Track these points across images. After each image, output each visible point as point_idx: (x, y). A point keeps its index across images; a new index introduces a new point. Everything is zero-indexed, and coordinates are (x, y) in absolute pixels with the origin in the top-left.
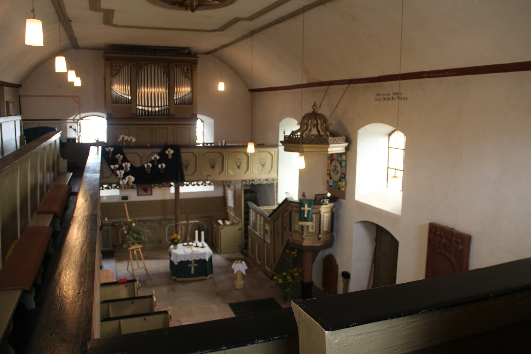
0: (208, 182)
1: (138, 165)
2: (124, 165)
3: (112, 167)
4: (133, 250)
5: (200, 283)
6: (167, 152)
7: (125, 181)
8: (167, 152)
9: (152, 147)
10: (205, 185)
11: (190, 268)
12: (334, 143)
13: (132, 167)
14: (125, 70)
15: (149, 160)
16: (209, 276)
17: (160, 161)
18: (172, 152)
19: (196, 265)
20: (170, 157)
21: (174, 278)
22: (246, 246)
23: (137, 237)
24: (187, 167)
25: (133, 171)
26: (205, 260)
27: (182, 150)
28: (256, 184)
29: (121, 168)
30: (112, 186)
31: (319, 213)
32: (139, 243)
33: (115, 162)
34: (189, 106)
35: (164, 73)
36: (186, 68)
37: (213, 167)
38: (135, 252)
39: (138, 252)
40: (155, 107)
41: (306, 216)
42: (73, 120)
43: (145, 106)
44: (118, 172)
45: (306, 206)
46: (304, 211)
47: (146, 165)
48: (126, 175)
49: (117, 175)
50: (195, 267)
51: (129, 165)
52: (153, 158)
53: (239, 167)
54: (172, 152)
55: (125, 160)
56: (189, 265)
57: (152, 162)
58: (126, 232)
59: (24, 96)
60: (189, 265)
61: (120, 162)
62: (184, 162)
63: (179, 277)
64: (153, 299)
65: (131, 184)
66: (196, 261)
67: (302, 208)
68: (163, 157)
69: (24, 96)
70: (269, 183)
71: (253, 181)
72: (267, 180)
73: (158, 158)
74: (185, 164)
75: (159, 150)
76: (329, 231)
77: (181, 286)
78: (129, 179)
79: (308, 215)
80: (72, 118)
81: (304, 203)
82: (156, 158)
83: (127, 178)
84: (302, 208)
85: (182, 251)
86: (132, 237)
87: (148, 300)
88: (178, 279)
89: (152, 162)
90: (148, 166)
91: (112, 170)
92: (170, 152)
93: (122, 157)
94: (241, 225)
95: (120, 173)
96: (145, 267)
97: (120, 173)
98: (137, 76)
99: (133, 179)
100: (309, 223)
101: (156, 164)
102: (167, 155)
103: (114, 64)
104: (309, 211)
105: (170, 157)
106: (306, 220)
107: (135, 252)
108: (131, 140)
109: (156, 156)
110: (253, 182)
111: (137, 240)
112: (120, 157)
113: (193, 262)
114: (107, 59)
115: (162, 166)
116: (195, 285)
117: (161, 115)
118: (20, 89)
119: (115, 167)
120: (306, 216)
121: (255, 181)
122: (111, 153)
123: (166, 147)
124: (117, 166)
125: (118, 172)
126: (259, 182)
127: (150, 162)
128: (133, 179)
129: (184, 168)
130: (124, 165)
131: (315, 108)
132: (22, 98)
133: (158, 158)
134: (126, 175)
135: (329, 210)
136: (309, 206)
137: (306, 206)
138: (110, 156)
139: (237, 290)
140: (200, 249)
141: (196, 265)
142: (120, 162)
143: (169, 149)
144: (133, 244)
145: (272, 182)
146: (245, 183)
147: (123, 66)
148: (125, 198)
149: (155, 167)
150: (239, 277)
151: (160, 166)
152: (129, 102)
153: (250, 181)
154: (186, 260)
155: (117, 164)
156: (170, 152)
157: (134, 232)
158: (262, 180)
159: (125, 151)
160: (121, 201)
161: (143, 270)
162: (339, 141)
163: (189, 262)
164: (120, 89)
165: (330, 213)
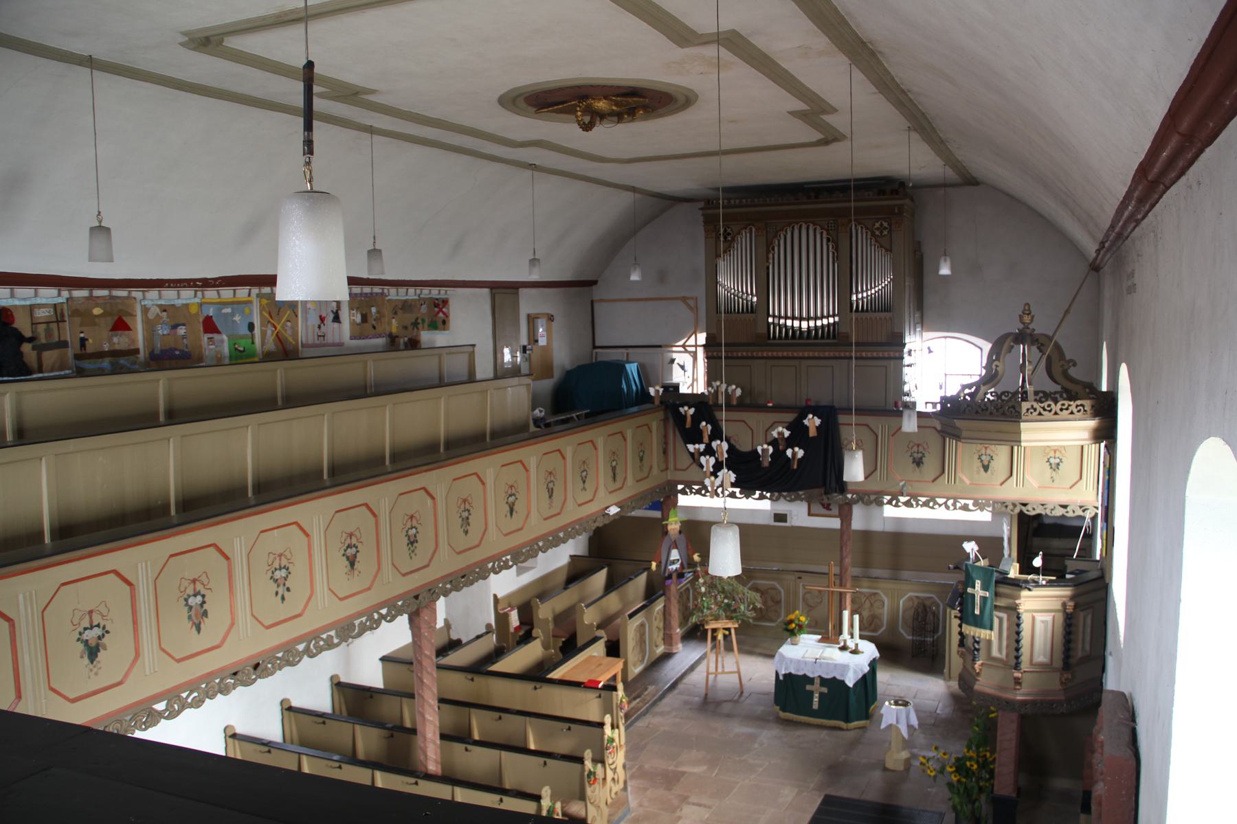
0: (903, 499)
1: (745, 447)
2: (714, 444)
3: (691, 447)
4: (714, 630)
5: (824, 734)
6: (806, 422)
8: (806, 422)
9: (778, 408)
10: (896, 506)
11: (811, 693)
12: (1040, 417)
13: (731, 450)
14: (745, 241)
15: (769, 440)
17: (790, 442)
18: (817, 421)
19: (825, 690)
20: (812, 433)
23: (728, 605)
26: (843, 682)
27: (842, 419)
28: (1032, 513)
29: (709, 451)
30: (691, 489)
31: (1013, 611)
32: (730, 618)
33: (695, 437)
34: (883, 315)
35: (828, 240)
36: (877, 225)
37: (918, 463)
38: (720, 637)
40: (780, 317)
41: (977, 612)
42: (684, 346)
43: (793, 318)
44: (703, 460)
45: (978, 584)
46: (973, 596)
47: (759, 449)
48: (718, 467)
49: (702, 467)
50: (821, 694)
51: (725, 446)
52: (775, 434)
53: (986, 468)
54: (817, 421)
55: (717, 434)
56: (808, 687)
57: (774, 443)
58: (703, 589)
59: (601, 300)
60: (808, 687)
61: (706, 439)
64: (603, 734)
66: (824, 682)
67: (969, 590)
68: (798, 434)
69: (601, 300)
70: (1071, 514)
71: (1025, 505)
72: (1065, 507)
73: (787, 433)
75: (790, 417)
76: (1058, 663)
79: (982, 611)
80: (681, 343)
81: (974, 575)
82: (781, 434)
84: (969, 590)
85: (805, 652)
86: (716, 603)
87: (598, 730)
88: (782, 714)
89: (774, 443)
91: (692, 455)
95: (707, 461)
96: (739, 672)
97: (707, 461)
98: (768, 252)
100: (983, 634)
102: (807, 428)
103: (877, 225)
104: (984, 599)
105: (812, 433)
106: (978, 622)
107: (720, 637)
109: (780, 429)
110: (1024, 509)
111: (725, 610)
113: (817, 681)
114: (710, 222)
115: (794, 454)
117: (823, 337)
118: (594, 287)
120: (977, 612)
121: (1029, 507)
122: (689, 419)
124: (702, 447)
125: (703, 460)
127: (769, 444)
130: (714, 444)
131: (1027, 319)
132: (596, 306)
133: (787, 433)
134: (718, 467)
135: (1058, 606)
136: (985, 588)
137: (978, 584)
138: (688, 425)
140: (851, 657)
141: (825, 690)
142: (706, 439)
143: (810, 416)
144: (717, 618)
145: (1079, 512)
147: (739, 233)
148: (780, 517)
149: (779, 455)
151: (789, 452)
152: (752, 310)
153: (1014, 505)
154: (801, 673)
155: (701, 442)
157: (723, 591)
158: (1050, 507)
160: (772, 523)
161: (734, 679)
162: (1078, 415)
163: (806, 679)
164: (734, 284)
165: (1060, 617)
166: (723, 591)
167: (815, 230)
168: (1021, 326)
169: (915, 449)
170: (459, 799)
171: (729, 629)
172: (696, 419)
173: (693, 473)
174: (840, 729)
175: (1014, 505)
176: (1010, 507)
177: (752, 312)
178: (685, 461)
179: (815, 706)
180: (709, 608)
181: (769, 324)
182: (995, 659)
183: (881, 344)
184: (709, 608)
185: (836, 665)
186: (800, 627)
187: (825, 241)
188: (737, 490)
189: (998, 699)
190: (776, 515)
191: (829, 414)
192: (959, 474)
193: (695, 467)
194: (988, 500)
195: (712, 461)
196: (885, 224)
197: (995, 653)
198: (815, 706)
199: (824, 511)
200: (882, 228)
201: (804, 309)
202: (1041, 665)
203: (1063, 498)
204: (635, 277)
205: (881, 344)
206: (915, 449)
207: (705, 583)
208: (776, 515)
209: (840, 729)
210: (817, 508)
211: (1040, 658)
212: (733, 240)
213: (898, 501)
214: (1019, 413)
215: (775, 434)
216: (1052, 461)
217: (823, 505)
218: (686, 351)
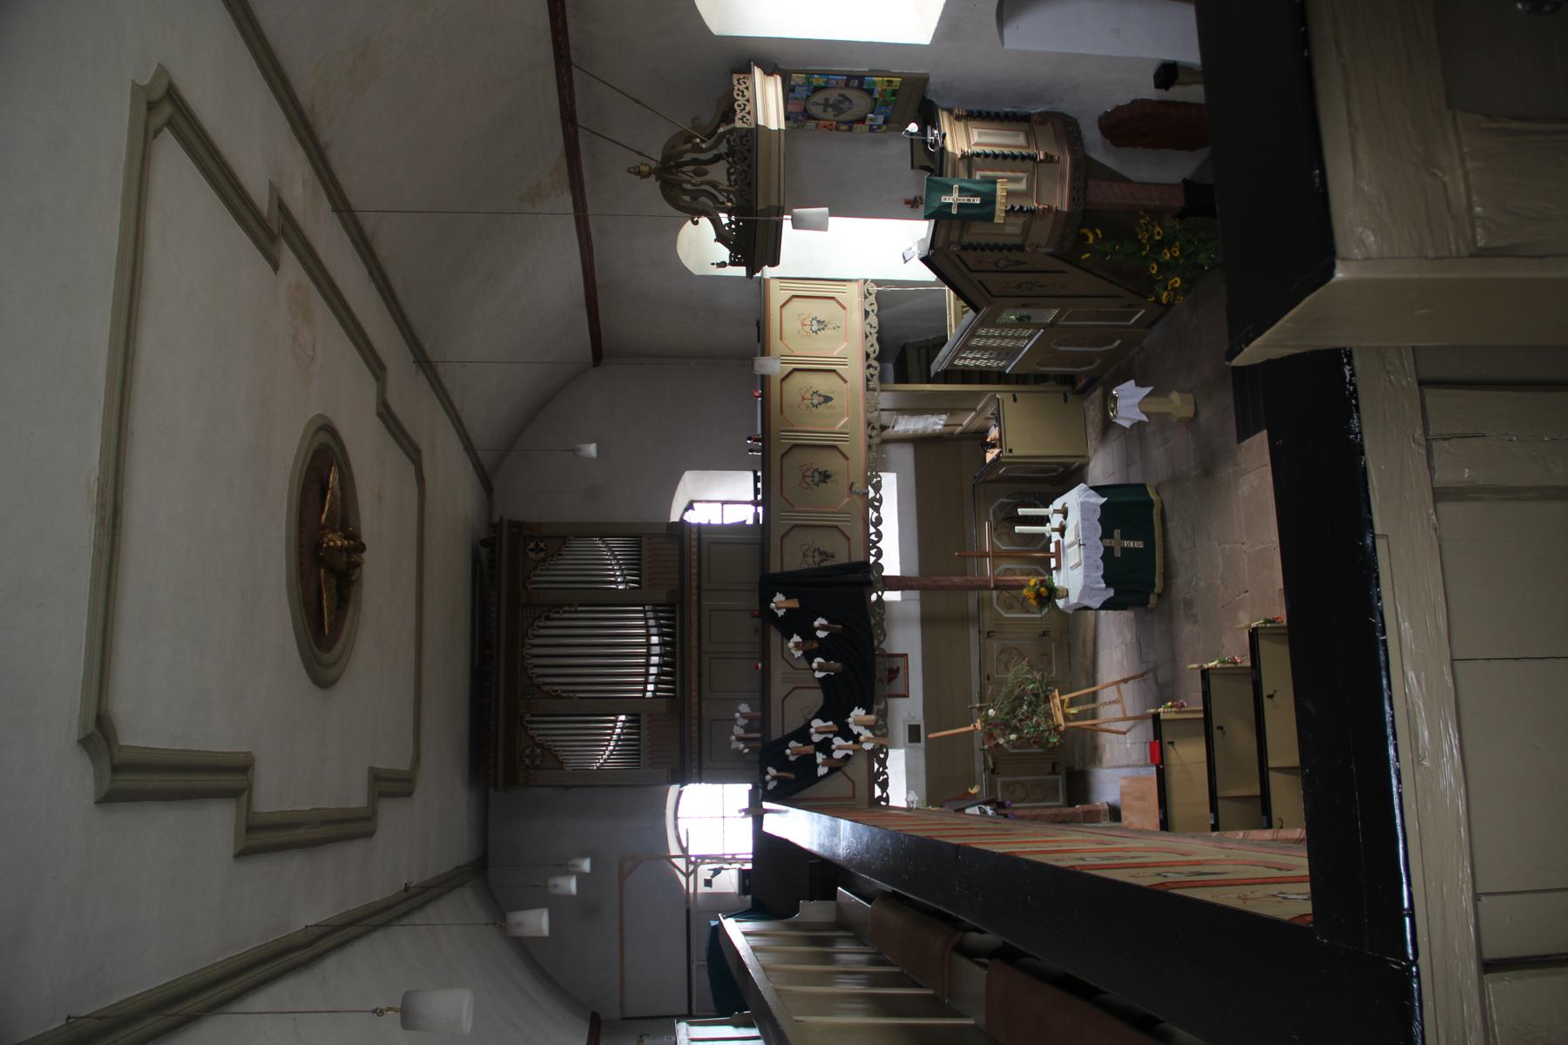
0: (872, 494)
1: (817, 698)
2: (816, 738)
3: (822, 771)
4: (1066, 717)
6: (781, 613)
7: (866, 734)
8: (781, 613)
9: (765, 656)
10: (880, 501)
11: (1123, 549)
16: (1153, 496)
17: (808, 634)
18: (779, 597)
19: (1117, 533)
20: (794, 603)
21: (1153, 599)
22: (1067, 380)
24: (825, 555)
25: (835, 710)
26: (1103, 506)
27: (775, 568)
28: (877, 347)
29: (825, 747)
30: (879, 774)
32: (1047, 700)
33: (808, 762)
35: (548, 618)
37: (826, 477)
38: (1073, 711)
39: (1072, 703)
41: (978, 201)
42: (687, 875)
44: (838, 755)
46: (960, 205)
47: (819, 675)
48: (846, 733)
49: (847, 757)
50: (1124, 537)
51: (817, 723)
52: (798, 654)
53: (828, 399)
54: (779, 597)
55: (803, 735)
56: (1118, 554)
57: (809, 656)
58: (1013, 737)
60: (1118, 554)
61: (810, 749)
62: (811, 562)
63: (1153, 585)
65: (872, 717)
67: (954, 211)
68: (796, 623)
70: (875, 307)
71: (868, 356)
72: (867, 314)
73: (796, 638)
74: (817, 559)
75: (775, 636)
76: (1025, 126)
77: (1180, 582)
78: (857, 723)
80: (683, 879)
82: (797, 645)
83: (856, 729)
85: (1074, 576)
88: (1158, 590)
89: (809, 656)
90: (821, 668)
91: (832, 771)
92: (780, 603)
93: (793, 744)
94: (1002, 392)
95: (840, 748)
97: (840, 748)
99: (858, 713)
101: (815, 645)
102: (789, 610)
103: (527, 761)
105: (794, 603)
106: (989, 200)
107: (1073, 711)
108: (743, 716)
109: (791, 645)
111: (1038, 706)
112: (793, 749)
113: (1108, 542)
115: (822, 628)
116: (1175, 538)
119: (824, 765)
121: (870, 350)
123: (767, 615)
124: (820, 757)
125: (838, 755)
126: (873, 339)
128: (858, 713)
129: (825, 564)
130: (816, 738)
132: (628, 1015)
133: (796, 638)
134: (846, 733)
135: (960, 126)
136: (948, 190)
137: (946, 199)
139: (1196, 414)
141: (1117, 533)
142: (810, 749)
144: (1049, 716)
146: (876, 379)
149: (824, 649)
150: (1158, 406)
151: (821, 634)
152: (634, 720)
153: (869, 366)
154: (1101, 564)
155: (814, 756)
156: (780, 603)
157: (1014, 710)
159: (776, 734)
163: (1107, 556)
166: (1014, 710)
167: (534, 656)
168: (653, 177)
169: (809, 480)
170: (1294, 759)
171: (1062, 702)
172: (783, 764)
173: (857, 770)
174: (1163, 509)
175: (869, 366)
176: (872, 371)
177: (638, 721)
178: (839, 779)
179: (1139, 545)
180: (1038, 724)
181: (655, 697)
182: (1030, 186)
183: (682, 550)
184: (1038, 724)
185: (1083, 519)
186: (1042, 582)
187: (549, 623)
188: (876, 707)
189: (1073, 180)
190: (911, 740)
191: (770, 584)
192: (837, 428)
193: (848, 769)
194: (867, 401)
195: (838, 741)
196: (532, 545)
197: (1022, 186)
198: (1139, 545)
199: (901, 675)
200: (537, 550)
201: (639, 655)
202: (1027, 139)
203: (856, 316)
204: (592, 449)
205: (682, 550)
206: (809, 480)
207: (1004, 736)
208: (911, 740)
209: (1163, 509)
210: (898, 682)
211: (1021, 140)
212: (541, 746)
213: (874, 499)
214: (749, 131)
215: (798, 654)
216: (815, 328)
217: (890, 680)
218: (695, 871)
